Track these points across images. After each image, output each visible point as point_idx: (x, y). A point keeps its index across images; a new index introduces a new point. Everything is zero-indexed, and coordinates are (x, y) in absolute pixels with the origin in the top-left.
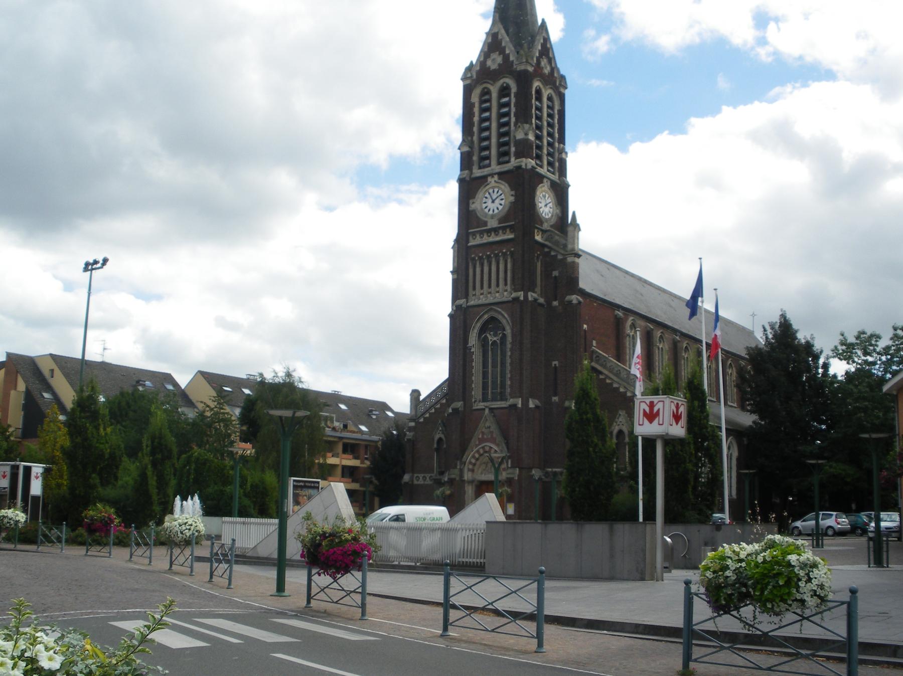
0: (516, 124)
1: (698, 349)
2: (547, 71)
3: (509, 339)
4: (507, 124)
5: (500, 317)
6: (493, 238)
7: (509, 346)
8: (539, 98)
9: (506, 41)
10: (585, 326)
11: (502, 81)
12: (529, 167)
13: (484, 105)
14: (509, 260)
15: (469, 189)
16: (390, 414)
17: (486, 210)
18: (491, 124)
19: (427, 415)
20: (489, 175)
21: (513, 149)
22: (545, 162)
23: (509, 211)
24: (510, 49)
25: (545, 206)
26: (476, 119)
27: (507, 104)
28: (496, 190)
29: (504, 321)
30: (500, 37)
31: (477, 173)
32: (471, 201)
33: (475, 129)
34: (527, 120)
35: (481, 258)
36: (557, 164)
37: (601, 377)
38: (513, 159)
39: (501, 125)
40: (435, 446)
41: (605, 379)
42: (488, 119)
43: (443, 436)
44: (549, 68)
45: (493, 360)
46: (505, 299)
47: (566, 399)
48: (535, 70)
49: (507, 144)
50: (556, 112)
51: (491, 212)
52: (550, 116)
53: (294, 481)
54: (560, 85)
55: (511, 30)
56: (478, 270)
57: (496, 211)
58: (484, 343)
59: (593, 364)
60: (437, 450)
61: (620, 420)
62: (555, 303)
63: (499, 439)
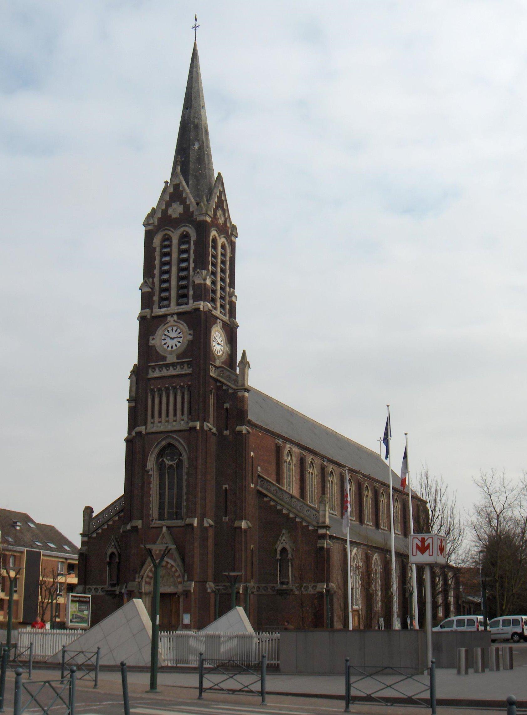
0: (195, 269)
1: (341, 473)
2: (221, 221)
3: (186, 464)
4: (186, 269)
5: (176, 444)
6: (172, 372)
7: (185, 470)
8: (215, 247)
10: (252, 454)
11: (182, 229)
12: (206, 309)
13: (165, 250)
14: (186, 393)
15: (148, 326)
16: (32, 525)
17: (165, 346)
18: (171, 268)
19: (100, 531)
20: (169, 315)
21: (191, 292)
22: (218, 305)
23: (187, 348)
24: (191, 200)
25: (218, 344)
26: (157, 262)
27: (187, 251)
28: (175, 329)
29: (181, 448)
30: (181, 188)
32: (151, 338)
33: (157, 272)
34: (205, 268)
35: (160, 390)
36: (228, 306)
37: (266, 499)
38: (191, 301)
39: (181, 270)
40: (108, 560)
41: (269, 502)
42: (168, 263)
43: (115, 551)
44: (223, 219)
45: (169, 483)
46: (183, 428)
47: (235, 520)
48: (212, 221)
49: (185, 287)
50: (228, 259)
51: (170, 348)
52: (223, 262)
53: (72, 596)
54: (232, 234)
55: (190, 183)
56: (157, 400)
57: (174, 348)
58: (161, 467)
59: (259, 488)
60: (109, 563)
61: (284, 538)
62: (226, 433)
63: (176, 555)
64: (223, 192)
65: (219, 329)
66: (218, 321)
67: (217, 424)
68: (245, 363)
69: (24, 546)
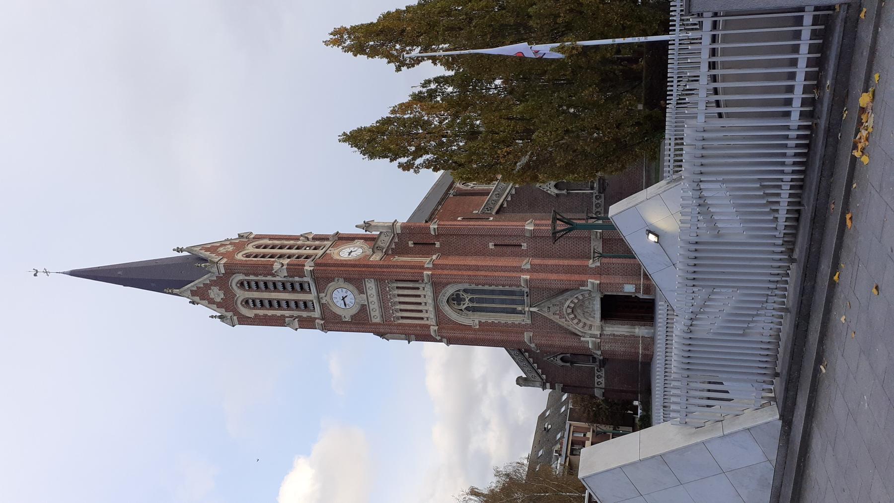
0: (273, 275)
2: (230, 248)
5: (448, 295)
9: (199, 282)
15: (332, 322)
16: (547, 414)
20: (319, 302)
24: (205, 279)
30: (195, 289)
31: (317, 314)
33: (279, 313)
37: (505, 205)
38: (305, 279)
40: (568, 364)
60: (572, 363)
62: (438, 245)
64: (204, 247)
65: (336, 251)
66: (328, 252)
67: (428, 254)
68: (367, 226)
69: (565, 423)
